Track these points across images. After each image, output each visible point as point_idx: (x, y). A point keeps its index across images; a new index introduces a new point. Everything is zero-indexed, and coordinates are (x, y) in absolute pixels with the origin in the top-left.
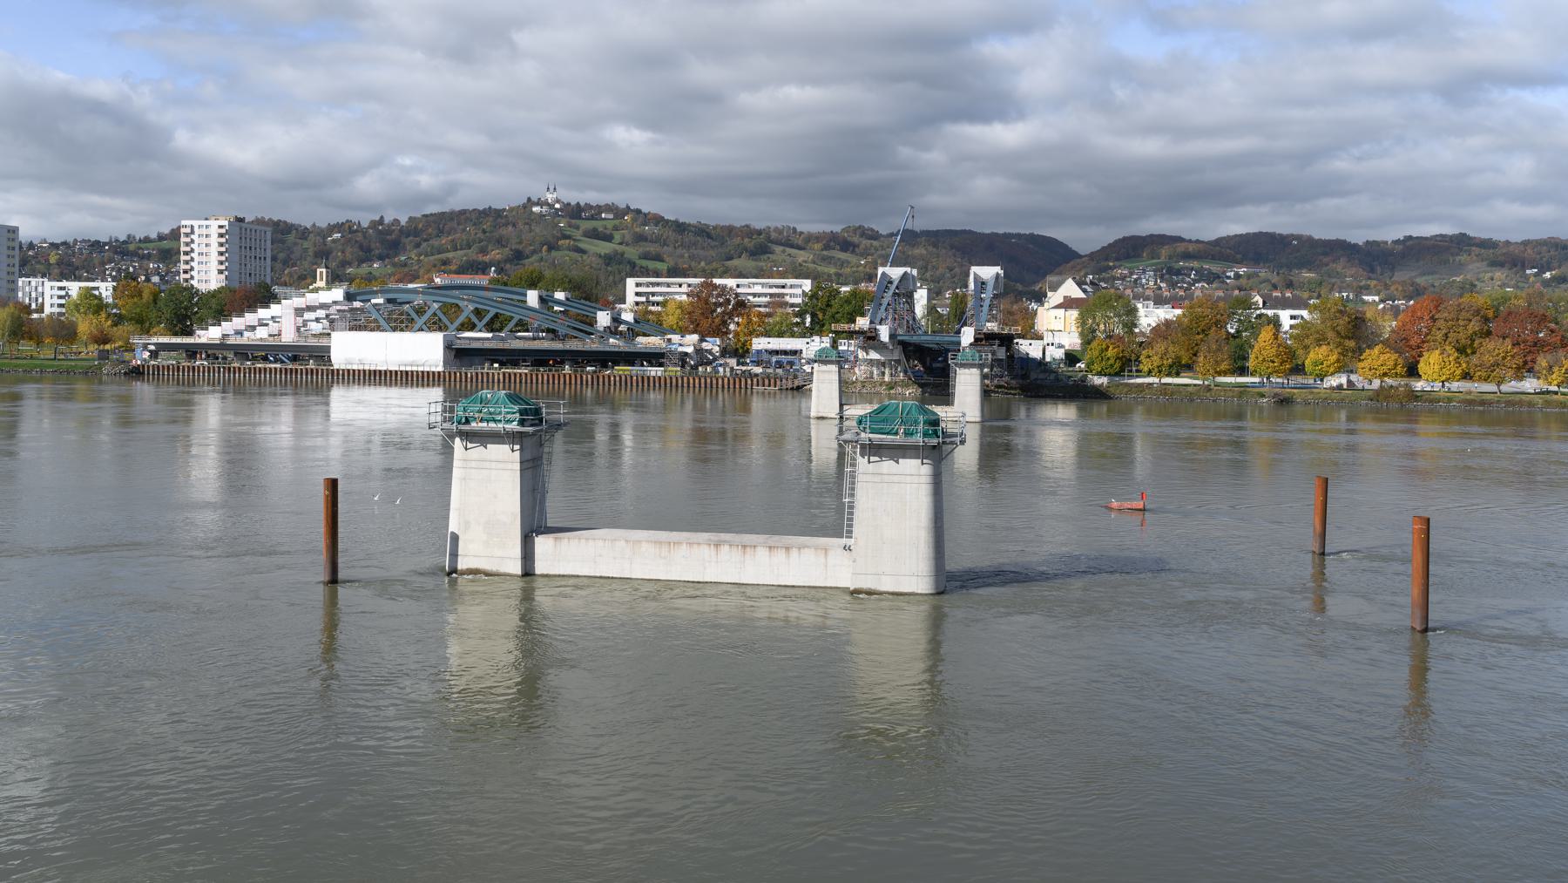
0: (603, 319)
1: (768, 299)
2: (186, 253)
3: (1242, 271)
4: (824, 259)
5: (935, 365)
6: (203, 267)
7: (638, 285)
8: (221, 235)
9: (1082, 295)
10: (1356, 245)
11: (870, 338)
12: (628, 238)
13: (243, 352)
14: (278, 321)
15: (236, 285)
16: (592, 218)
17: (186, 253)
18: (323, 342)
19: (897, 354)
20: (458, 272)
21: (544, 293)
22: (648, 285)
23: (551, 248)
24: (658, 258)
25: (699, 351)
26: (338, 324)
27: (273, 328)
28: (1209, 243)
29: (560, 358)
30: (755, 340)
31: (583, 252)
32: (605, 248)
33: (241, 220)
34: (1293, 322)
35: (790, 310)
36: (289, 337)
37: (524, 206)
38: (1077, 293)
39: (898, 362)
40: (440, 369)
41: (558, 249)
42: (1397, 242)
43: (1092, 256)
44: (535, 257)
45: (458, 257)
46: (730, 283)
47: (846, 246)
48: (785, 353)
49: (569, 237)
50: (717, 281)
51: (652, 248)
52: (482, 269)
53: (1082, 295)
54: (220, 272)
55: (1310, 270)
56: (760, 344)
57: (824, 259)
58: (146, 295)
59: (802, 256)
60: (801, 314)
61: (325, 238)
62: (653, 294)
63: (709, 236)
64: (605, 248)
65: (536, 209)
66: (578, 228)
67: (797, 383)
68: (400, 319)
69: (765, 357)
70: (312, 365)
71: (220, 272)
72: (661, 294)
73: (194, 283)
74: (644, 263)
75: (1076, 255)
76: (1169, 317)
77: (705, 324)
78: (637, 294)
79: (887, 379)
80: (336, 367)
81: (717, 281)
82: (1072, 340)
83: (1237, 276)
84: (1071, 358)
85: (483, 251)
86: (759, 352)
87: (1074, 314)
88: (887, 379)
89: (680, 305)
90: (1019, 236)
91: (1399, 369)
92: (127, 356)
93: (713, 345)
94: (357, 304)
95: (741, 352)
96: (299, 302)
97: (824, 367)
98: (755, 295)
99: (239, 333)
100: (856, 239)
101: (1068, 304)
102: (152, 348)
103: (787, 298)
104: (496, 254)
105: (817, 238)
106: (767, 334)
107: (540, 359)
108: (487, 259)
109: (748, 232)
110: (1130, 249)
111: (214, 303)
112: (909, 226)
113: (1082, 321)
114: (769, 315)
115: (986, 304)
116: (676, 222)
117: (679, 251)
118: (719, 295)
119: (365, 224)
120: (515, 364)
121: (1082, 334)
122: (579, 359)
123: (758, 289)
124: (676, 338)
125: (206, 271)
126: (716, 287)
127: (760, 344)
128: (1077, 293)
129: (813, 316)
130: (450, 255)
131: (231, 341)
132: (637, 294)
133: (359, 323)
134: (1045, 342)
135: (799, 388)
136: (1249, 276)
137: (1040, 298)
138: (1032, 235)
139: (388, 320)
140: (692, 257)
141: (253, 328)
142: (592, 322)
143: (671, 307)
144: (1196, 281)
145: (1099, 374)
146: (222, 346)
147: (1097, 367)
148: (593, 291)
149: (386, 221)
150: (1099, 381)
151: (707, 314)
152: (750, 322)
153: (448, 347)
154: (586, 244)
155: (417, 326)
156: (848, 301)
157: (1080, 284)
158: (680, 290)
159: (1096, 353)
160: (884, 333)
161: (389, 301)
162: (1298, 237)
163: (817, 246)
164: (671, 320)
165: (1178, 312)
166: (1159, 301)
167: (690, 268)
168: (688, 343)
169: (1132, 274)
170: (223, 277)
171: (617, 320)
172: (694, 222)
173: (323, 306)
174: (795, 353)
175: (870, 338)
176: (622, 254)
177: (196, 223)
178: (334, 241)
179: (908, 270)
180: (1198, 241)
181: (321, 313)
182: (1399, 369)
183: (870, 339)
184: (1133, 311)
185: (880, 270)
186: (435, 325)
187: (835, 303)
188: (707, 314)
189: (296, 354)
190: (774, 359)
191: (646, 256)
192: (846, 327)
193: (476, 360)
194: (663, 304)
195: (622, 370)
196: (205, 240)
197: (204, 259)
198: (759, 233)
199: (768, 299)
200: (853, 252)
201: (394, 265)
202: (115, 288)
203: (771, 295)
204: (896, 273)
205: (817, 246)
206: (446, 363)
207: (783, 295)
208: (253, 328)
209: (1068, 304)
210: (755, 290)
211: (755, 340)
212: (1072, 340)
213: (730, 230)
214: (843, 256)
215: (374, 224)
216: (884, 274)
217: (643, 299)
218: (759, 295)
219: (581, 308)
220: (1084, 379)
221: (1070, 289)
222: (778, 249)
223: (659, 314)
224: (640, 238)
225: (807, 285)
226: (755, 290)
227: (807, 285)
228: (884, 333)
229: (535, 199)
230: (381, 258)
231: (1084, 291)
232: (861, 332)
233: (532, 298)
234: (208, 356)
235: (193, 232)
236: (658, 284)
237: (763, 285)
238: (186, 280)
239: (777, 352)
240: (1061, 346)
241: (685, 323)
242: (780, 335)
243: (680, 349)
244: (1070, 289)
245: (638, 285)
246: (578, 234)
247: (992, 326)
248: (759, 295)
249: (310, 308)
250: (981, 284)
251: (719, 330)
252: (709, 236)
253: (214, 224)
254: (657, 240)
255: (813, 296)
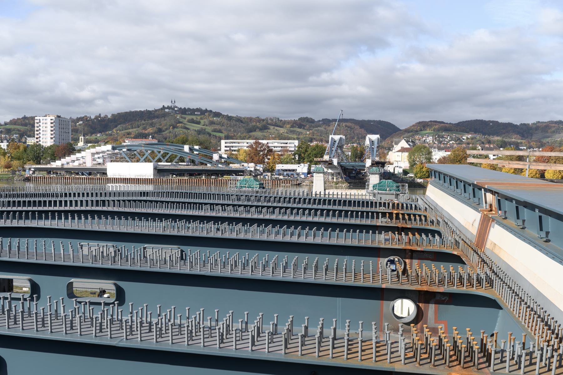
0: (216, 157)
1: (280, 149)
2: (37, 131)
3: (469, 136)
4: (291, 131)
5: (351, 175)
6: (44, 137)
7: (226, 143)
8: (52, 123)
9: (409, 147)
10: (516, 125)
11: (329, 164)
12: (207, 123)
13: (69, 171)
14: (85, 158)
15: (58, 144)
16: (191, 114)
17: (37, 131)
18: (103, 167)
19: (340, 170)
20: (135, 138)
21: (191, 147)
22: (230, 143)
23: (174, 127)
24: (220, 131)
25: (256, 170)
26: (107, 160)
27: (81, 161)
28: (455, 124)
29: (199, 173)
30: (277, 166)
31: (188, 129)
32: (197, 127)
33: (59, 117)
34: (495, 157)
35: (290, 153)
36: (89, 164)
37: (162, 109)
38: (406, 146)
39: (339, 173)
40: (152, 177)
41: (177, 127)
42: (534, 124)
43: (407, 131)
44: (167, 131)
45: (134, 131)
46: (264, 142)
47: (300, 126)
48: (290, 170)
49: (181, 123)
50: (260, 141)
51: (217, 127)
52: (145, 136)
53: (409, 147)
54: (52, 138)
55: (498, 136)
56: (279, 167)
57: (291, 131)
58: (22, 148)
59: (282, 130)
60: (294, 155)
61: (76, 123)
62: (232, 147)
63: (242, 122)
64: (197, 127)
65: (167, 110)
66: (185, 118)
67: (298, 182)
68: (133, 156)
69: (281, 172)
70: (98, 176)
71: (52, 138)
72: (236, 147)
73: (41, 143)
74: (215, 134)
75: (398, 130)
76: (445, 155)
77: (256, 159)
78: (226, 147)
79: (335, 180)
80: (109, 177)
81: (260, 141)
82: (406, 165)
83: (468, 138)
84: (405, 172)
85: (145, 129)
86: (279, 170)
87: (406, 154)
88: (335, 180)
89: (245, 151)
90: (374, 121)
91: (537, 175)
92: (23, 173)
93: (260, 167)
94: (117, 151)
95: (272, 170)
96: (93, 150)
97: (318, 175)
98: (274, 147)
99: (68, 163)
100: (304, 123)
101: (403, 150)
102: (33, 169)
103: (288, 148)
104: (150, 130)
105: (288, 122)
106: (281, 163)
107: (191, 173)
108: (146, 132)
109: (259, 120)
110: (423, 126)
111: (50, 151)
112: (341, 118)
113: (410, 157)
114: (281, 155)
115: (375, 150)
116: (227, 116)
117: (229, 128)
118: (262, 147)
119: (93, 117)
120: (184, 175)
121: (410, 162)
122: (210, 173)
123: (276, 144)
124: (246, 165)
125: (46, 137)
126: (260, 143)
127: (279, 167)
128: (406, 146)
129: (300, 155)
130: (130, 130)
131: (66, 166)
132: (226, 147)
133: (115, 158)
134: (394, 165)
135: (299, 184)
136: (472, 139)
137: (390, 149)
138: (380, 121)
139: (129, 158)
140: (235, 131)
141: (74, 161)
142: (212, 158)
143: (241, 152)
144: (450, 141)
145: (420, 178)
146: (62, 169)
147: (419, 175)
148: (209, 147)
149: (102, 116)
150: (419, 181)
151: (256, 155)
152: (274, 158)
153: (155, 168)
154: (190, 125)
155: (141, 160)
156: (315, 149)
157: (407, 142)
158: (244, 145)
159: (419, 170)
160: (335, 162)
161: (128, 150)
162: (493, 122)
163: (288, 126)
164: (241, 157)
165: (449, 153)
166: (440, 149)
167: (234, 136)
168: (251, 166)
169: (423, 137)
170: (53, 140)
171: (221, 157)
172: (234, 115)
173: (103, 152)
174: (294, 170)
175: (329, 164)
176: (205, 130)
177: (41, 118)
178: (80, 125)
179: (342, 136)
180: (450, 124)
181: (101, 155)
182: (537, 175)
183: (329, 164)
184: (430, 153)
185: (331, 136)
186: (147, 160)
187: (309, 151)
188: (256, 155)
189: (90, 172)
190: (285, 173)
191: (215, 131)
192: (319, 159)
193: (165, 174)
194: (238, 151)
195: (233, 177)
196: (45, 125)
197: (45, 133)
198: (263, 120)
199: (280, 149)
200: (304, 128)
201: (106, 135)
202: (8, 146)
203: (281, 147)
204: (337, 138)
205: (288, 126)
206: (154, 175)
207: (286, 147)
208: (74, 161)
209: (403, 150)
210: (275, 144)
211: (277, 166)
212: (406, 165)
213: (251, 119)
214: (299, 130)
215: (96, 118)
216: (332, 138)
217: (228, 149)
218: (277, 147)
219: (206, 152)
220: (414, 180)
221: (403, 144)
222: (272, 127)
223: (237, 154)
224: (212, 123)
225: (296, 143)
226: (275, 144)
227: (296, 143)
228: (335, 162)
229: (166, 106)
230: (100, 132)
231: (409, 145)
232: (325, 162)
233: (186, 148)
234: (54, 173)
235: (40, 122)
236: (234, 143)
237: (278, 143)
238: (37, 142)
239: (286, 170)
240: (400, 167)
241: (247, 158)
242: (287, 163)
243: (248, 169)
244: (403, 144)
245: (226, 143)
246: (185, 121)
247: (377, 159)
248: (277, 147)
249: (98, 153)
250: (372, 142)
251: (262, 162)
252: (242, 122)
253: (49, 119)
254: (219, 124)
255: (299, 147)
